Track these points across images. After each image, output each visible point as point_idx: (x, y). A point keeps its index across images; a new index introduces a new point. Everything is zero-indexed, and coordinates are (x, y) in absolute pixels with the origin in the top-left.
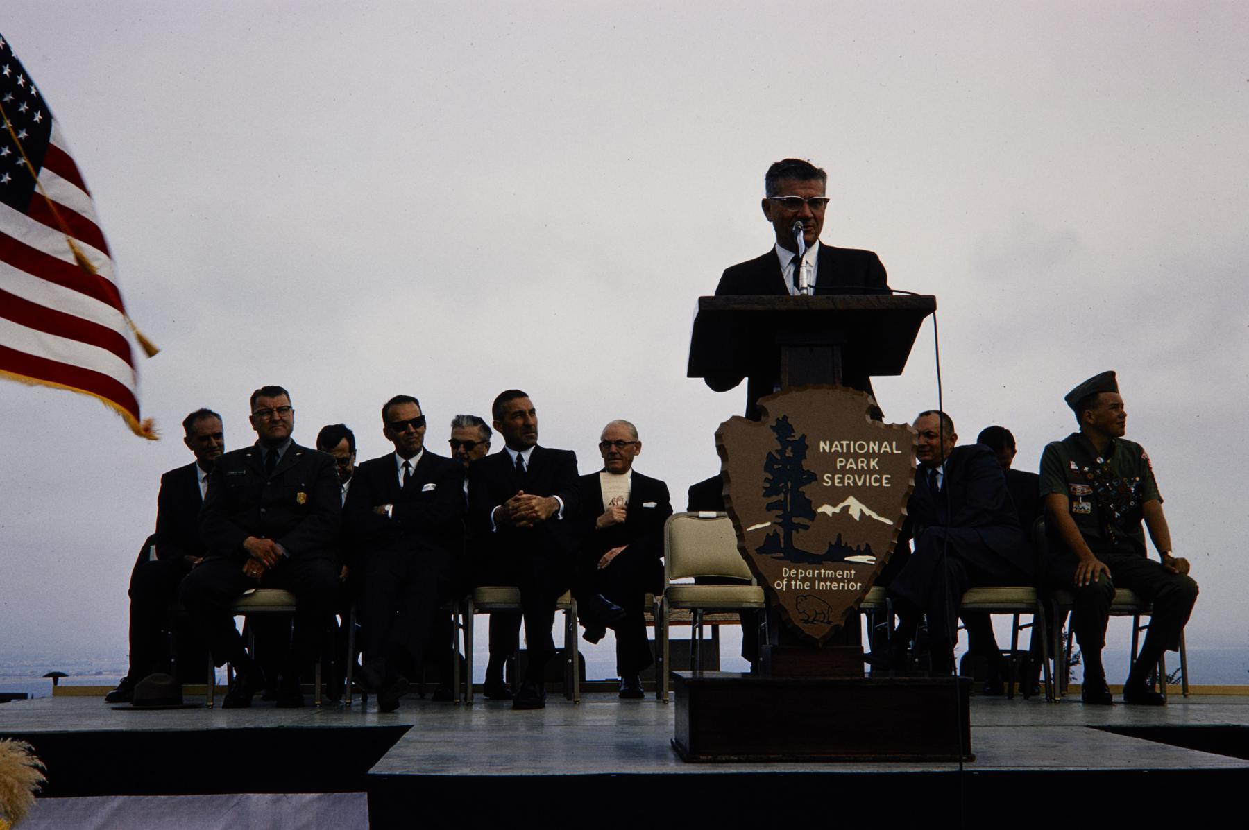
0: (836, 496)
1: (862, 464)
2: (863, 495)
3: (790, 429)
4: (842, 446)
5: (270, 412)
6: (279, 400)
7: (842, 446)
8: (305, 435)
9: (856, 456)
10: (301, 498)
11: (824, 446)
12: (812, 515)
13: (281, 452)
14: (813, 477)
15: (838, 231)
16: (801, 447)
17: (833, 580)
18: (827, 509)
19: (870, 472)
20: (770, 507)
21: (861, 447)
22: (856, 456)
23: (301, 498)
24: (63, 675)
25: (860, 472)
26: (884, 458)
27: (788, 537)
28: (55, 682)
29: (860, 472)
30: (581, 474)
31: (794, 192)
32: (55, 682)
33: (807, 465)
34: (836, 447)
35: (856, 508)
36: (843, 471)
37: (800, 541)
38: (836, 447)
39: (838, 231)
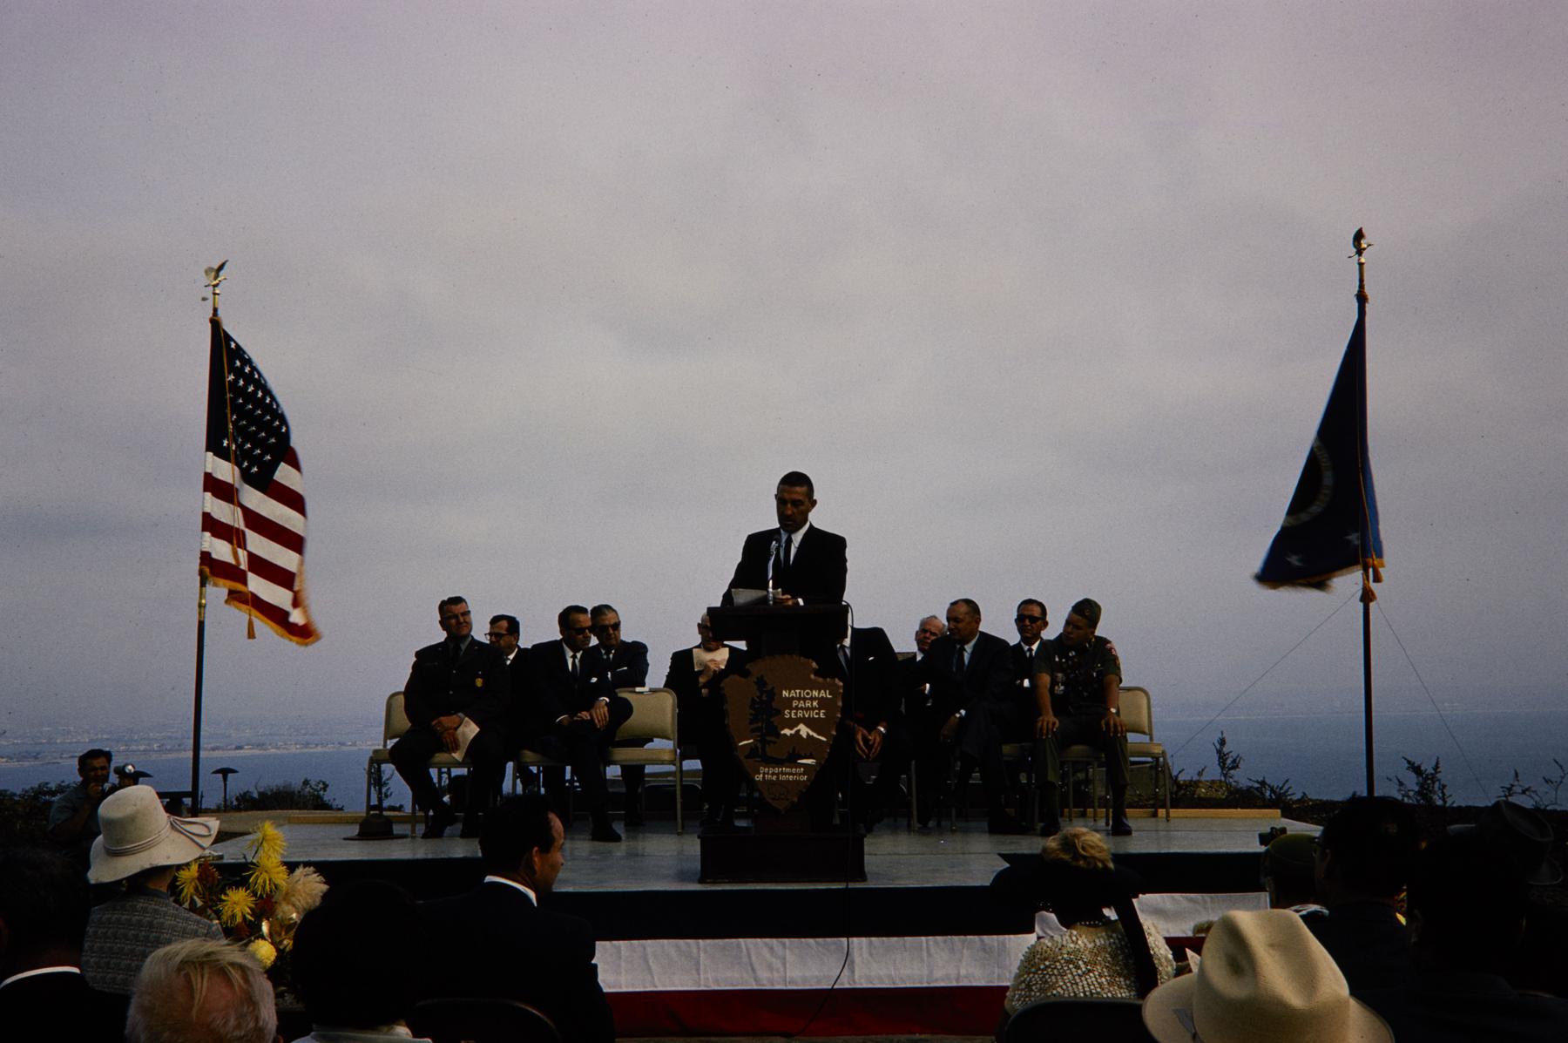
0: (792, 723)
1: (808, 704)
2: (809, 723)
3: (765, 684)
5: (456, 617)
6: (458, 609)
8: (480, 631)
9: (805, 699)
10: (479, 682)
11: (785, 694)
12: (778, 735)
13: (463, 647)
14: (779, 712)
15: (819, 518)
16: (773, 694)
17: (788, 774)
18: (787, 732)
19: (813, 709)
20: (753, 731)
22: (805, 699)
23: (479, 682)
24: (233, 771)
25: (807, 709)
26: (822, 701)
27: (763, 749)
28: (225, 779)
29: (807, 709)
30: (600, 946)
31: (795, 493)
32: (225, 779)
33: (774, 705)
34: (793, 694)
35: (804, 730)
36: (797, 708)
37: (770, 750)
38: (793, 694)
39: (819, 518)
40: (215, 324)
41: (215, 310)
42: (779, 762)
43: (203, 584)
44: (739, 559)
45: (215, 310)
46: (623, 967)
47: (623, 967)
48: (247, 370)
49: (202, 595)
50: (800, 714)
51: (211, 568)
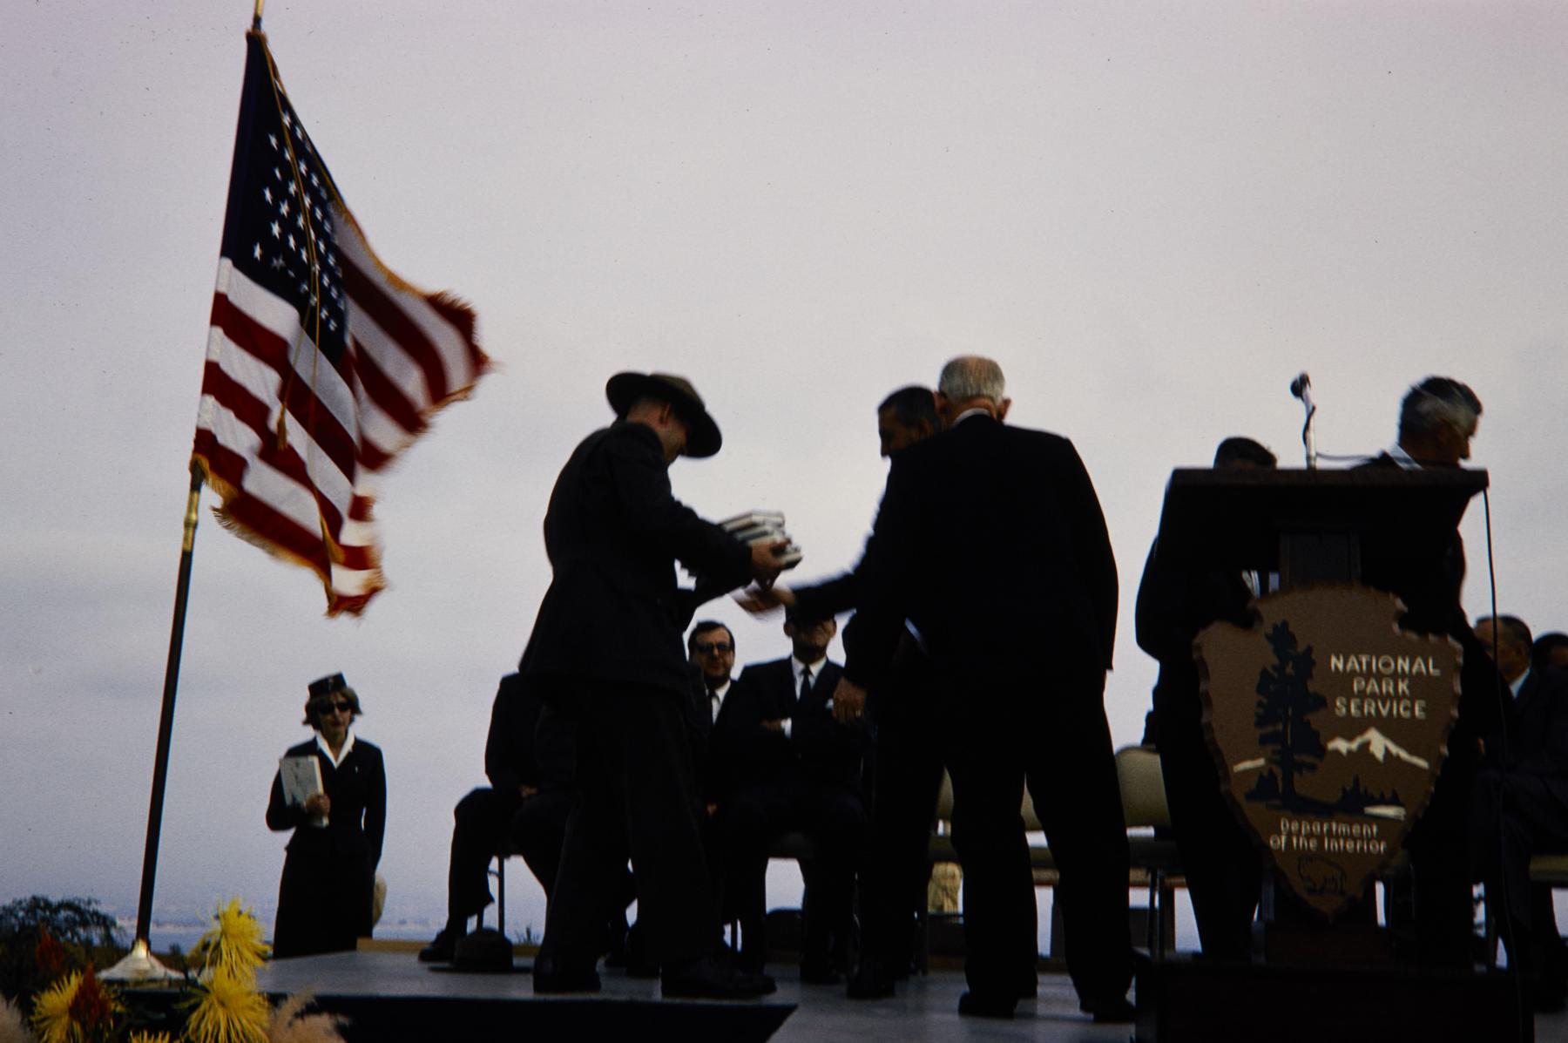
0: (1353, 728)
1: (1388, 687)
2: (1389, 727)
4: (1360, 664)
7: (1360, 664)
9: (1379, 677)
11: (1336, 663)
12: (1321, 751)
14: (1322, 703)
16: (1307, 663)
18: (1341, 745)
19: (1398, 697)
20: (1264, 740)
21: (1386, 665)
25: (1384, 698)
26: (1416, 681)
29: (1384, 698)
34: (1353, 663)
35: (1378, 744)
36: (1362, 695)
37: (1304, 785)
38: (1353, 663)
41: (257, 20)
42: (1323, 811)
45: (257, 20)
50: (1370, 708)
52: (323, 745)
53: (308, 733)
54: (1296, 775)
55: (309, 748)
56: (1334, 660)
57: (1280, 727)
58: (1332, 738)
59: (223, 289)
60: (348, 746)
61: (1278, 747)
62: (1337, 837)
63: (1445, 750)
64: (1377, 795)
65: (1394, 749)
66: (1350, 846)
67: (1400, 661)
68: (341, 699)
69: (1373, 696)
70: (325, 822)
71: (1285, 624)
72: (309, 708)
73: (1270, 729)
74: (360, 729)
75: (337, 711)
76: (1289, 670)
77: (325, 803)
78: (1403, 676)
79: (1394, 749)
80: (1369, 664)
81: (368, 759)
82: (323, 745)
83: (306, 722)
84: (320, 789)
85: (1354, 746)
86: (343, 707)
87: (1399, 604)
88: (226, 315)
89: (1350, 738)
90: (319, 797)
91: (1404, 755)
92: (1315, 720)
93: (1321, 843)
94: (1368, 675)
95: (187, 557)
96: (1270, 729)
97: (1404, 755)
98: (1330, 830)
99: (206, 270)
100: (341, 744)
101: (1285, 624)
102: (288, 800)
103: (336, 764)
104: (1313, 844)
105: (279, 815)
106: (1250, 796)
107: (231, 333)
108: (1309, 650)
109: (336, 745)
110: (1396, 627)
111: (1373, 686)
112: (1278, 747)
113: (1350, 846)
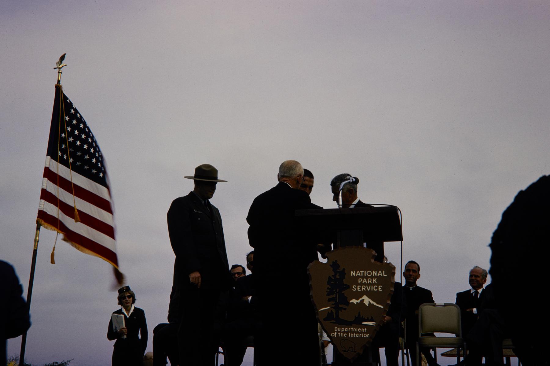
0: (358, 295)
1: (370, 281)
2: (370, 294)
4: (361, 273)
7: (361, 273)
9: (367, 277)
11: (353, 273)
12: (348, 303)
14: (348, 287)
16: (343, 274)
18: (354, 301)
19: (373, 284)
20: (329, 300)
21: (369, 273)
22: (367, 277)
25: (369, 285)
26: (379, 278)
29: (369, 285)
34: (358, 273)
35: (367, 300)
36: (361, 284)
37: (343, 315)
38: (358, 273)
40: (58, 88)
41: (59, 81)
42: (348, 324)
43: (38, 229)
44: (325, 208)
45: (59, 81)
46: (400, 351)
47: (400, 351)
48: (82, 126)
49: (37, 235)
50: (364, 289)
51: (44, 218)
52: (124, 311)
53: (119, 307)
54: (340, 311)
55: (119, 312)
56: (352, 272)
57: (334, 296)
58: (351, 300)
59: (47, 166)
60: (132, 310)
61: (334, 303)
62: (353, 333)
63: (389, 302)
64: (366, 318)
65: (372, 302)
66: (357, 335)
67: (374, 272)
68: (128, 294)
69: (365, 284)
70: (125, 337)
71: (336, 261)
72: (119, 298)
73: (331, 297)
74: (137, 305)
75: (127, 299)
76: (338, 277)
77: (125, 331)
78: (375, 277)
79: (372, 302)
80: (364, 273)
81: (139, 313)
82: (124, 311)
83: (119, 304)
84: (124, 326)
85: (359, 301)
86: (129, 297)
87: (374, 252)
88: (48, 174)
89: (358, 299)
90: (123, 328)
91: (375, 304)
92: (346, 293)
93: (348, 335)
94: (363, 277)
95: (35, 252)
96: (331, 297)
97: (375, 304)
98: (351, 330)
99: (42, 160)
100: (130, 310)
101: (336, 261)
102: (114, 328)
103: (128, 317)
104: (345, 335)
105: (111, 336)
106: (325, 319)
107: (50, 179)
108: (344, 269)
109: (128, 310)
110: (373, 261)
111: (365, 281)
112: (334, 303)
113: (357, 335)
